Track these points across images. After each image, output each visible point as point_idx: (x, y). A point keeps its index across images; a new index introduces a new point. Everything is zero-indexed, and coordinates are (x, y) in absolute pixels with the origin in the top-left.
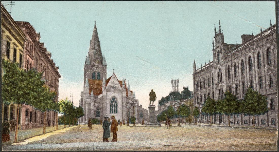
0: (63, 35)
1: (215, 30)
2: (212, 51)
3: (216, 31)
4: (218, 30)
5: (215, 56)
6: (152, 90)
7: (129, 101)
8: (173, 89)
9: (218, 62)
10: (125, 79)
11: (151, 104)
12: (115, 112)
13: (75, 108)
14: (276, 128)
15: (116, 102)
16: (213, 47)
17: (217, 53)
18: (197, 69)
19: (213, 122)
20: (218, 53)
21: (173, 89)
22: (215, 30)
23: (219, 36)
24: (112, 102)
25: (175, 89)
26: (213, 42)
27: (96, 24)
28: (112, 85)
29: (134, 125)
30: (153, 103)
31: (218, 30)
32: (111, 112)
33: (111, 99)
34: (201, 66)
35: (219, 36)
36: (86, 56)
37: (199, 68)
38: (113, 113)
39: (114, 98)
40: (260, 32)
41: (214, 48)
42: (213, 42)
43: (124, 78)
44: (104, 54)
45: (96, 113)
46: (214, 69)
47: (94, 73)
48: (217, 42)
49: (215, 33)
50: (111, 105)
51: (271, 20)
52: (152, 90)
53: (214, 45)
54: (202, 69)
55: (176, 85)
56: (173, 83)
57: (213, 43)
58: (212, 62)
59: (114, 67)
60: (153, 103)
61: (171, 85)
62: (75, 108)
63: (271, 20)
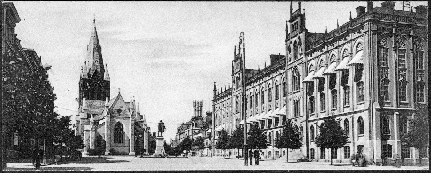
0: (55, 41)
1: (291, 9)
2: (285, 43)
3: (293, 11)
5: (234, 82)
6: (161, 121)
7: (138, 128)
8: (195, 114)
10: (134, 101)
11: (160, 135)
12: (120, 142)
14: (11, 149)
16: (287, 35)
17: (292, 46)
18: (217, 94)
19: (268, 156)
21: (195, 114)
24: (116, 129)
28: (117, 109)
29: (238, 159)
30: (161, 134)
33: (115, 126)
34: (224, 90)
36: (82, 67)
37: (230, 88)
40: (348, 20)
41: (289, 37)
43: (133, 99)
44: (106, 65)
48: (294, 28)
49: (292, 13)
52: (161, 121)
53: (289, 32)
54: (222, 95)
55: (200, 109)
56: (195, 106)
57: (287, 30)
58: (220, 94)
59: (120, 81)
60: (161, 134)
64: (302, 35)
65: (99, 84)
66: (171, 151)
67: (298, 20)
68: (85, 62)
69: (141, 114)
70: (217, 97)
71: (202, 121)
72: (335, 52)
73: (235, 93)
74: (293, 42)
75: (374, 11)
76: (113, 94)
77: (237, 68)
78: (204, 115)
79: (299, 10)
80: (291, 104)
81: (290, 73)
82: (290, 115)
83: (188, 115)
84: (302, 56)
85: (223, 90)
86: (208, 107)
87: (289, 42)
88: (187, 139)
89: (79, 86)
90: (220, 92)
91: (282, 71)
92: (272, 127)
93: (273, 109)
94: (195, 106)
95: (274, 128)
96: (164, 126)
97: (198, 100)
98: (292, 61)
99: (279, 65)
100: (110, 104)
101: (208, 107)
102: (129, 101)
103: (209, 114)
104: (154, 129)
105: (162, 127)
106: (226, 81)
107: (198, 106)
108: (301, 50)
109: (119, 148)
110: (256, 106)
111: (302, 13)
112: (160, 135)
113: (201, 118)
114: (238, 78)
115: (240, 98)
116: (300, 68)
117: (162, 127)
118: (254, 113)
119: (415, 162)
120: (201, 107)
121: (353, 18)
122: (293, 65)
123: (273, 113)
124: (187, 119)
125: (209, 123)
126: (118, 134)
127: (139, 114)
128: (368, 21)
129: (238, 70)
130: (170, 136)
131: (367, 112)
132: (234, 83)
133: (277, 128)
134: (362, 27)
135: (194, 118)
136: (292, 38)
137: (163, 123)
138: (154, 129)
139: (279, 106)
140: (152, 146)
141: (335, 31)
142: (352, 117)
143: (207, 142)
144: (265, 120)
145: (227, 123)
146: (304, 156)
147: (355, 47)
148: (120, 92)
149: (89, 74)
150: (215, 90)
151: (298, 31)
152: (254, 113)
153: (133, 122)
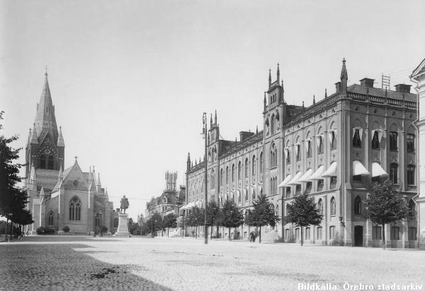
1: (270, 80)
2: (263, 115)
3: (272, 82)
4: (274, 79)
5: (267, 123)
6: (125, 197)
9: (213, 162)
13: (27, 208)
15: (78, 205)
16: (265, 107)
20: (272, 117)
22: (270, 80)
23: (276, 89)
24: (72, 204)
25: (171, 188)
26: (265, 99)
27: (347, 68)
31: (274, 79)
32: (70, 219)
35: (276, 89)
38: (73, 219)
39: (75, 199)
41: (268, 109)
42: (265, 99)
44: (60, 128)
45: (48, 220)
46: (178, 189)
47: (43, 156)
48: (273, 100)
49: (270, 84)
50: (70, 209)
51: (344, 61)
57: (265, 102)
59: (76, 153)
61: (165, 182)
62: (27, 208)
63: (344, 61)
64: (280, 109)
65: (51, 150)
66: (135, 230)
67: (277, 91)
68: (34, 125)
69: (102, 187)
70: (191, 170)
71: (173, 197)
72: (311, 128)
73: (267, 139)
74: (271, 115)
75: (348, 90)
76: (68, 163)
77: (213, 139)
78: (178, 189)
79: (278, 81)
80: (267, 180)
81: (268, 146)
82: (267, 192)
83: (159, 189)
84: (280, 131)
85: (198, 163)
86: (181, 181)
87: (266, 115)
88: (157, 216)
89: (27, 152)
90: (194, 165)
91: (260, 145)
92: (324, 189)
93: (327, 164)
94: (167, 178)
95: (329, 192)
96: (128, 203)
97: (172, 171)
98: (270, 135)
99: (302, 117)
100: (65, 174)
101: (181, 181)
102: (88, 171)
103: (183, 188)
104: (117, 205)
105: (125, 203)
106: (198, 155)
107: (171, 178)
108: (279, 124)
109: (73, 226)
110: (331, 150)
111: (281, 84)
112: (123, 212)
113: (174, 193)
114: (214, 150)
115: (216, 172)
116: (277, 142)
117: (125, 203)
118: (315, 165)
119: (404, 244)
120: (175, 178)
121: (328, 96)
122: (270, 140)
123: (303, 177)
124: (159, 194)
125: (182, 200)
126: (74, 210)
127: (99, 186)
128: (342, 100)
129: (214, 141)
130: (138, 212)
131: (338, 192)
132: (268, 125)
133: (320, 194)
134: (335, 104)
135: (166, 193)
136: (270, 110)
137: (127, 199)
138: (117, 205)
139: (324, 162)
140: (115, 223)
141: (322, 102)
142: (326, 197)
143: (179, 220)
144: (292, 186)
145: (195, 202)
146: (279, 237)
147: (330, 125)
148: (76, 161)
149: (39, 140)
150: (189, 162)
151: (276, 103)
152: (315, 165)
153: (93, 196)
